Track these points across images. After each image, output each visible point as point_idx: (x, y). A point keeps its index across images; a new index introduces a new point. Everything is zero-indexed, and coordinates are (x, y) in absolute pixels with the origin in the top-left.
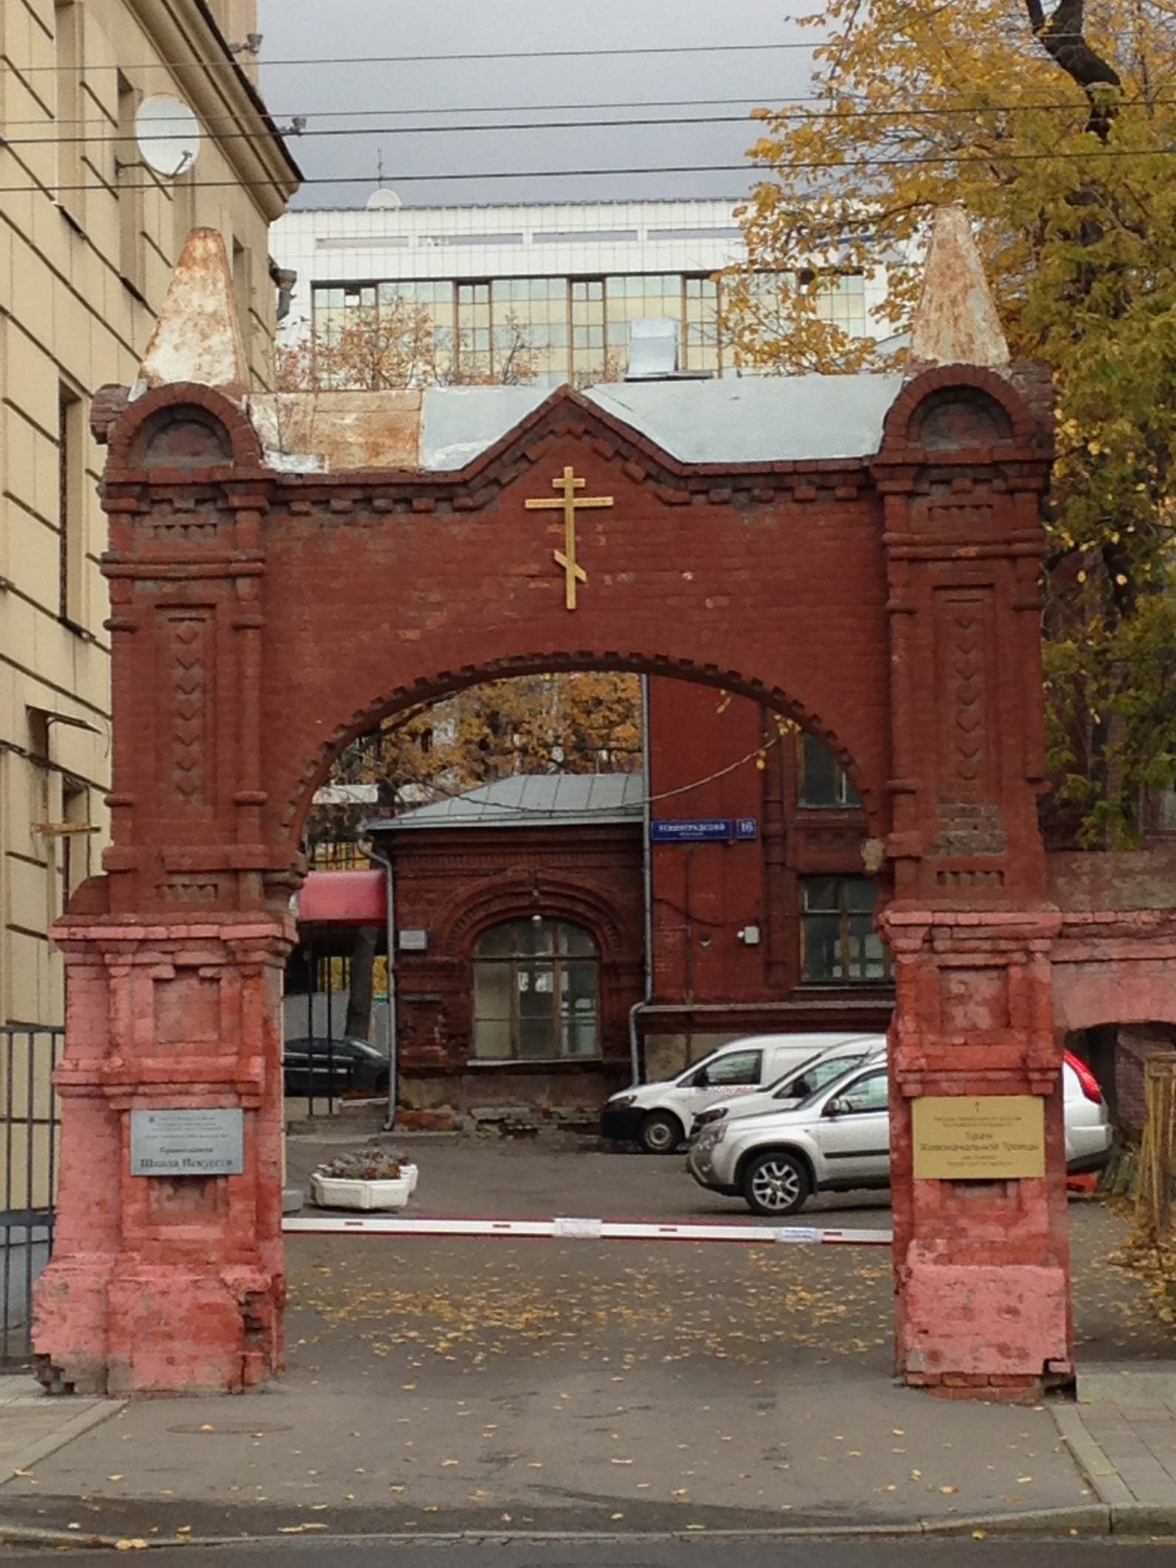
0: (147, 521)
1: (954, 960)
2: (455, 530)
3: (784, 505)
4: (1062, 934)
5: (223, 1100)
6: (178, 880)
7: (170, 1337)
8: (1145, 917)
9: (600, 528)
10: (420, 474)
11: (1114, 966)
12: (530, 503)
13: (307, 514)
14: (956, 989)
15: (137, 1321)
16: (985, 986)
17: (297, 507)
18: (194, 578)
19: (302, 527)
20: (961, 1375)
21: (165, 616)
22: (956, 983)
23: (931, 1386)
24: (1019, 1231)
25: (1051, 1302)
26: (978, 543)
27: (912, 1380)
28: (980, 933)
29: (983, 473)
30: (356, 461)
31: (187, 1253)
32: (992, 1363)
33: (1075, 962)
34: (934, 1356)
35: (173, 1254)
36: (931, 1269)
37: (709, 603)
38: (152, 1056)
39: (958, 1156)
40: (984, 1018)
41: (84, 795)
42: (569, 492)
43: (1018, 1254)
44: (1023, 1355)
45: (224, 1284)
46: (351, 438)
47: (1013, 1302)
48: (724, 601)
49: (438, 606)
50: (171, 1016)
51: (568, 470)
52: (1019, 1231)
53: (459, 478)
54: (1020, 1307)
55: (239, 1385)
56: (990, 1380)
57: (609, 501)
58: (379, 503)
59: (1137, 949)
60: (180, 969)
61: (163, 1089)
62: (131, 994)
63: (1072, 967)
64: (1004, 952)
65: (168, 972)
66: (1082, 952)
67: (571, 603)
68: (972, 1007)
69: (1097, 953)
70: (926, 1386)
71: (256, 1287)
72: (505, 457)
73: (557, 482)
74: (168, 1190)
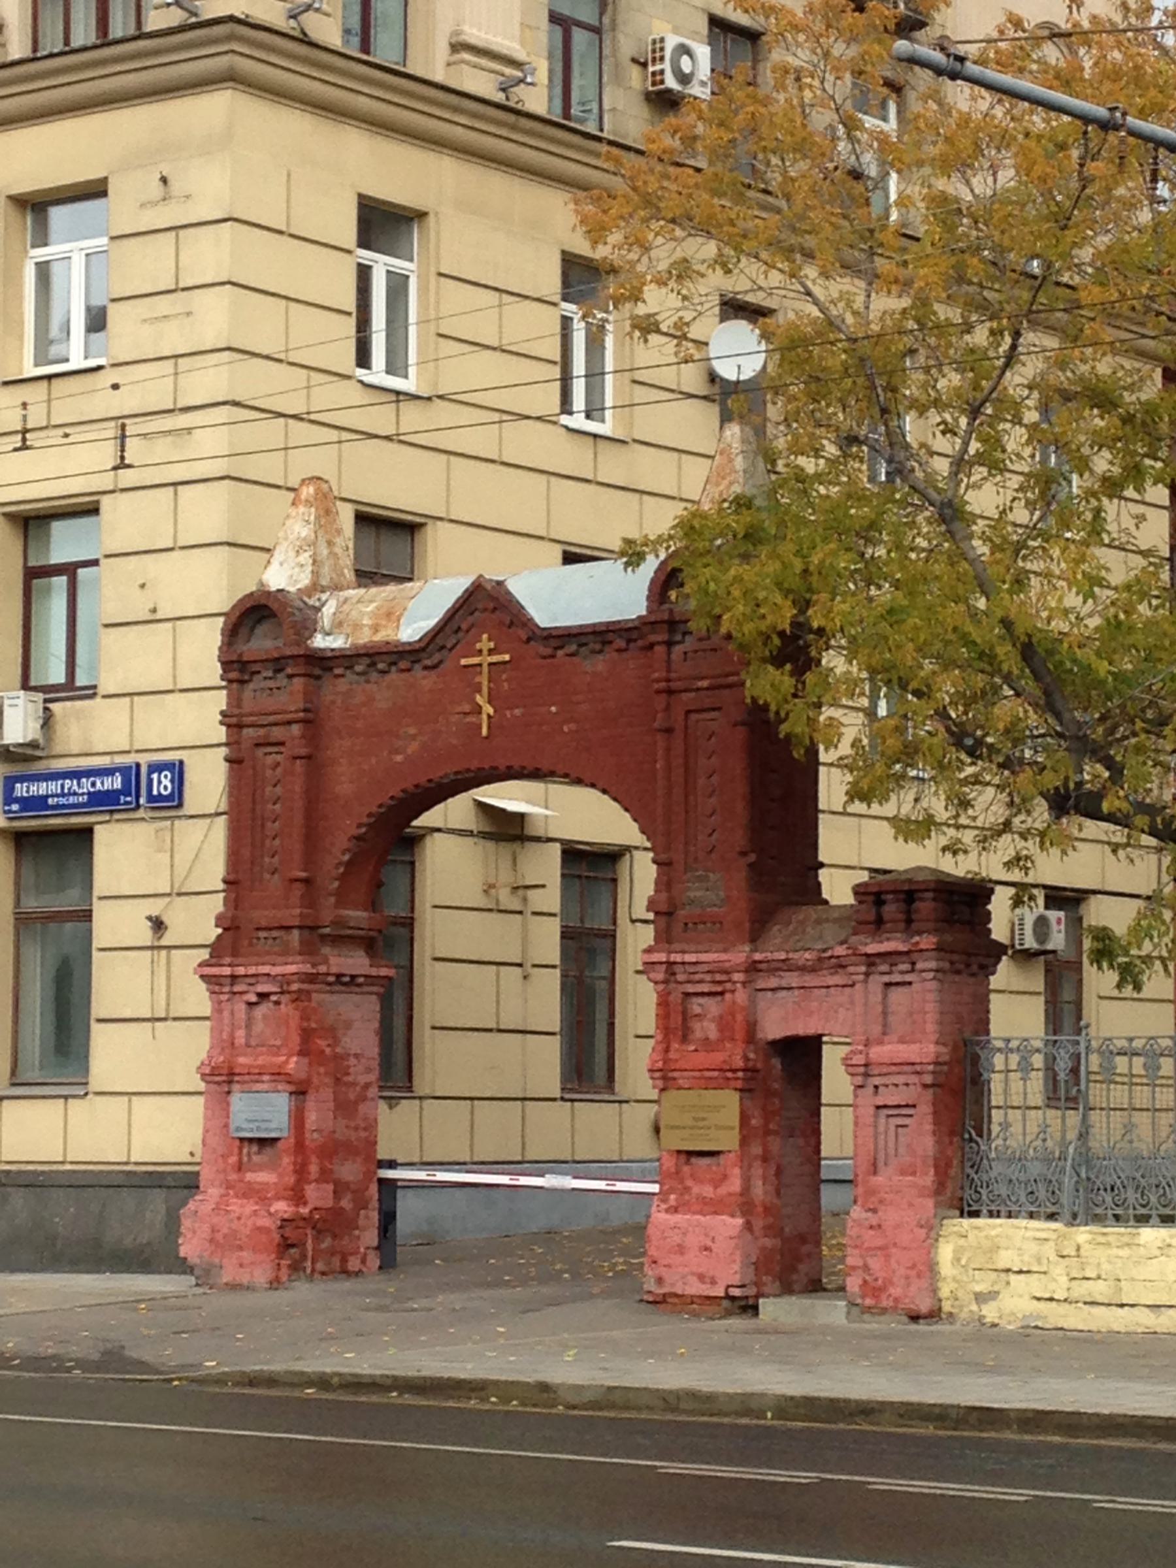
0: (251, 686)
1: (690, 988)
2: (424, 682)
3: (610, 654)
4: (753, 968)
5: (280, 1087)
6: (262, 934)
7: (241, 1248)
8: (807, 955)
9: (504, 677)
10: (399, 644)
11: (796, 992)
12: (463, 662)
13: (342, 676)
14: (697, 1010)
15: (225, 1236)
17: (337, 671)
18: (276, 724)
19: (342, 685)
20: (676, 1295)
21: (260, 752)
22: (696, 1006)
23: (660, 1302)
24: (723, 1190)
25: (733, 1242)
26: (713, 677)
27: (646, 1297)
28: (699, 968)
29: (394, 658)
30: (365, 637)
31: (258, 1192)
32: (695, 1288)
33: (772, 990)
34: (660, 1281)
36: (663, 1216)
37: (566, 729)
38: (245, 1055)
39: (686, 1133)
40: (713, 1032)
41: (628, 856)
42: (485, 652)
43: (714, 1207)
44: (713, 1282)
45: (270, 1214)
46: (366, 621)
47: (709, 1243)
48: (573, 726)
49: (414, 737)
50: (258, 1027)
51: (485, 636)
52: (723, 1190)
53: (417, 646)
54: (713, 1246)
55: (275, 1284)
56: (693, 1300)
57: (507, 657)
58: (381, 666)
59: (809, 980)
60: (260, 995)
61: (247, 1078)
62: (232, 1013)
63: (769, 994)
64: (720, 982)
65: (254, 999)
66: (773, 982)
67: (484, 732)
68: (705, 1024)
69: (784, 983)
70: (655, 1302)
71: (286, 1216)
72: (447, 629)
73: (478, 646)
74: (255, 1148)
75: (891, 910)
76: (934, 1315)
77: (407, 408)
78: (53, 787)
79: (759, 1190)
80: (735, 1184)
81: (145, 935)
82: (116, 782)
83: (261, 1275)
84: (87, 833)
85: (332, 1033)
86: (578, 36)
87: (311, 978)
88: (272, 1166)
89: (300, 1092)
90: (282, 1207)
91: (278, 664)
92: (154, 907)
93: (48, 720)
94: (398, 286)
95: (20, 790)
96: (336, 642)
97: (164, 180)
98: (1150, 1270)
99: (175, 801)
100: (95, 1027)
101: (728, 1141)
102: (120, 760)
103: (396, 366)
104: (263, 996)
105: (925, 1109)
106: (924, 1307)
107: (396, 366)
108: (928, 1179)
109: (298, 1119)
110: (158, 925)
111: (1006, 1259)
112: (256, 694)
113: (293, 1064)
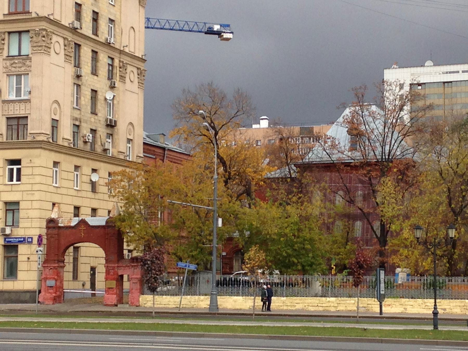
4: (118, 266)
16: (112, 271)
30: (66, 225)
32: (110, 304)
35: (49, 293)
40: (112, 274)
43: (113, 294)
50: (50, 272)
55: (53, 304)
75: (135, 260)
76: (139, 306)
77: (58, 189)
78: (12, 240)
79: (118, 292)
80: (115, 291)
81: (27, 260)
82: (23, 239)
83: (51, 303)
84: (17, 245)
85: (59, 273)
86: (75, 133)
87: (58, 266)
88: (53, 290)
89: (56, 280)
90: (54, 295)
91: (54, 228)
92: (28, 256)
93: (12, 230)
94: (56, 171)
95: (7, 240)
96: (62, 225)
97: (31, 160)
98: (164, 300)
99: (31, 242)
100: (18, 272)
101: (114, 286)
102: (23, 236)
103: (56, 183)
104: (51, 269)
105: (138, 283)
106: (138, 305)
107: (56, 183)
108: (139, 291)
109: (56, 284)
110: (29, 258)
111: (148, 300)
112: (50, 231)
113: (56, 277)
